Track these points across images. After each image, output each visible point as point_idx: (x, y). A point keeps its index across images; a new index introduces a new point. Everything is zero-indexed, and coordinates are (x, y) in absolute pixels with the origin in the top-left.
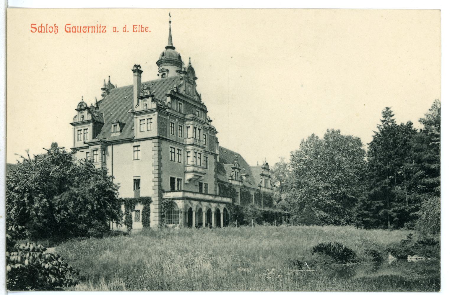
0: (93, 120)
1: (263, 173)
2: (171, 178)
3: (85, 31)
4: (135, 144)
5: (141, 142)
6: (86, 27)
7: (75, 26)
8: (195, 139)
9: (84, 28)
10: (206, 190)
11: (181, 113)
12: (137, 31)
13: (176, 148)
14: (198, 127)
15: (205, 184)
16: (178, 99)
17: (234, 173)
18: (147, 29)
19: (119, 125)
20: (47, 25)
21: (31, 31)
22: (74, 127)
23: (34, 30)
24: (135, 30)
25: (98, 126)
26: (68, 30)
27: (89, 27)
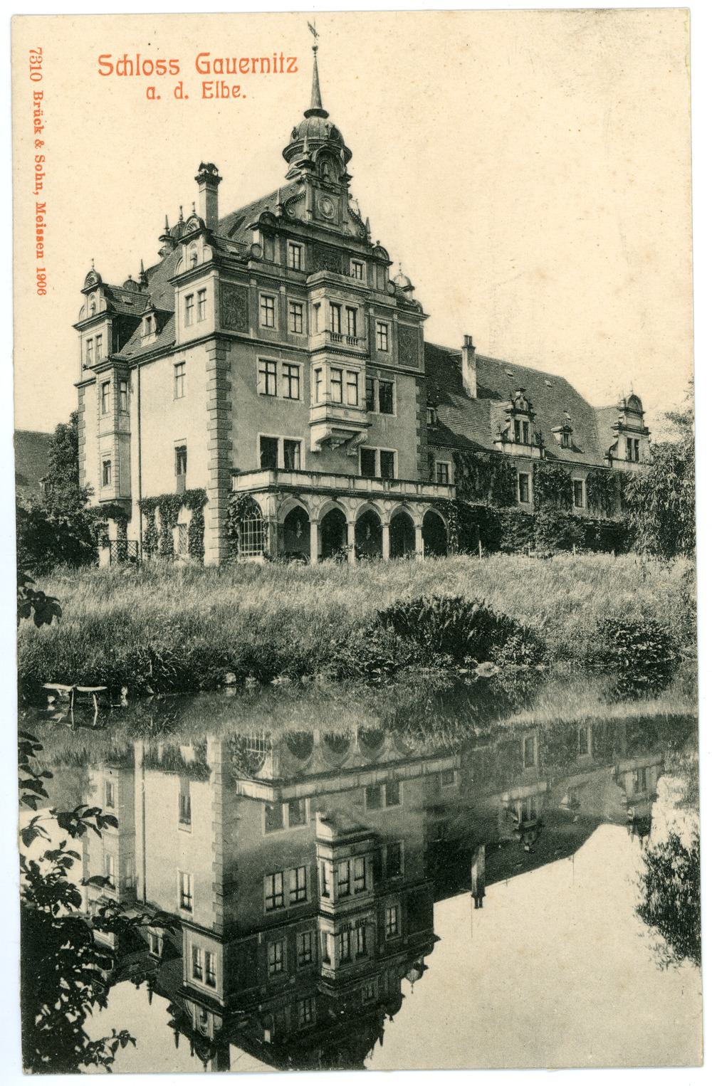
0: (110, 312)
1: (620, 423)
2: (263, 439)
3: (245, 69)
4: (177, 358)
5: (189, 352)
6: (247, 60)
7: (220, 58)
8: (336, 336)
9: (244, 63)
10: (441, 480)
11: (298, 271)
12: (212, 96)
13: (281, 361)
14: (345, 304)
15: (382, 452)
16: (286, 235)
17: (512, 425)
18: (236, 90)
19: (155, 316)
20: (138, 56)
21: (100, 72)
23: (106, 70)
24: (208, 93)
25: (123, 328)
26: (204, 67)
27: (254, 60)
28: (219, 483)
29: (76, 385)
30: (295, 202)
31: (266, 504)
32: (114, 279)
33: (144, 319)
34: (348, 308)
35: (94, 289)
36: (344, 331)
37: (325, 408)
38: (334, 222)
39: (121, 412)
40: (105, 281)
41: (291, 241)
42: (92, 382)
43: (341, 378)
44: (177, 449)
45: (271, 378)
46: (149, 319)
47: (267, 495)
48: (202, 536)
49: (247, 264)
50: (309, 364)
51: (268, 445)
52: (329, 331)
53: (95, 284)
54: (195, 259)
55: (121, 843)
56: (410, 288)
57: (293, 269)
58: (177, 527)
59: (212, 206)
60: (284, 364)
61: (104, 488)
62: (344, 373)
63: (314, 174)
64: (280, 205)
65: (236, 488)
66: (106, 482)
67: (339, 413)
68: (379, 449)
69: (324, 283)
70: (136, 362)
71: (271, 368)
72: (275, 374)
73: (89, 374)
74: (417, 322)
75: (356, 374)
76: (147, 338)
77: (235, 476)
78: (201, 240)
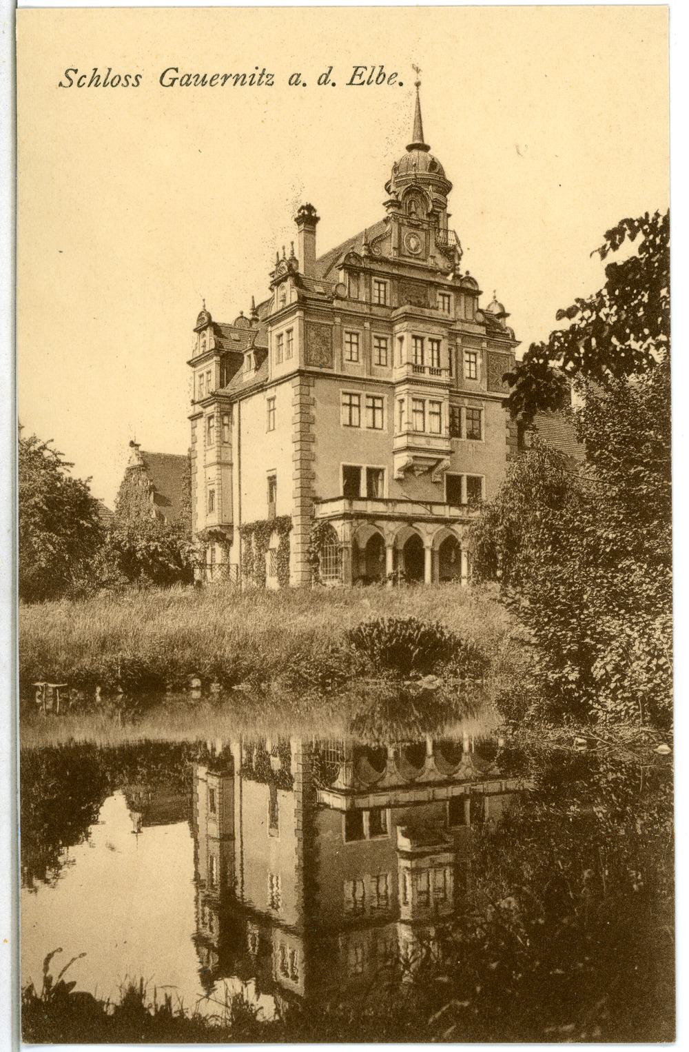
0: (218, 348)
4: (270, 393)
8: (418, 368)
11: (384, 306)
13: (364, 393)
14: (427, 336)
22: (193, 369)
23: (66, 82)
25: (229, 362)
28: (302, 511)
29: (189, 418)
30: (381, 241)
31: (342, 530)
32: (224, 317)
33: (245, 356)
34: (431, 340)
35: (205, 329)
36: (428, 362)
37: (405, 437)
38: (420, 257)
39: (224, 443)
40: (214, 319)
41: (376, 278)
42: (200, 415)
43: (424, 407)
44: (270, 478)
45: (355, 410)
46: (249, 356)
47: (342, 522)
48: (288, 560)
49: (332, 303)
50: (394, 395)
51: (351, 475)
52: (412, 364)
53: (206, 323)
54: (284, 301)
55: (221, 846)
56: (503, 315)
57: (379, 305)
58: (269, 552)
59: (309, 248)
60: (368, 397)
61: (209, 515)
62: (427, 402)
63: (401, 212)
64: (365, 244)
65: (318, 515)
66: (211, 509)
67: (420, 442)
68: (465, 474)
69: (407, 317)
70: (237, 397)
71: (355, 400)
72: (359, 406)
73: (198, 409)
74: (508, 349)
75: (439, 403)
76: (248, 374)
77: (318, 503)
78: (289, 282)
